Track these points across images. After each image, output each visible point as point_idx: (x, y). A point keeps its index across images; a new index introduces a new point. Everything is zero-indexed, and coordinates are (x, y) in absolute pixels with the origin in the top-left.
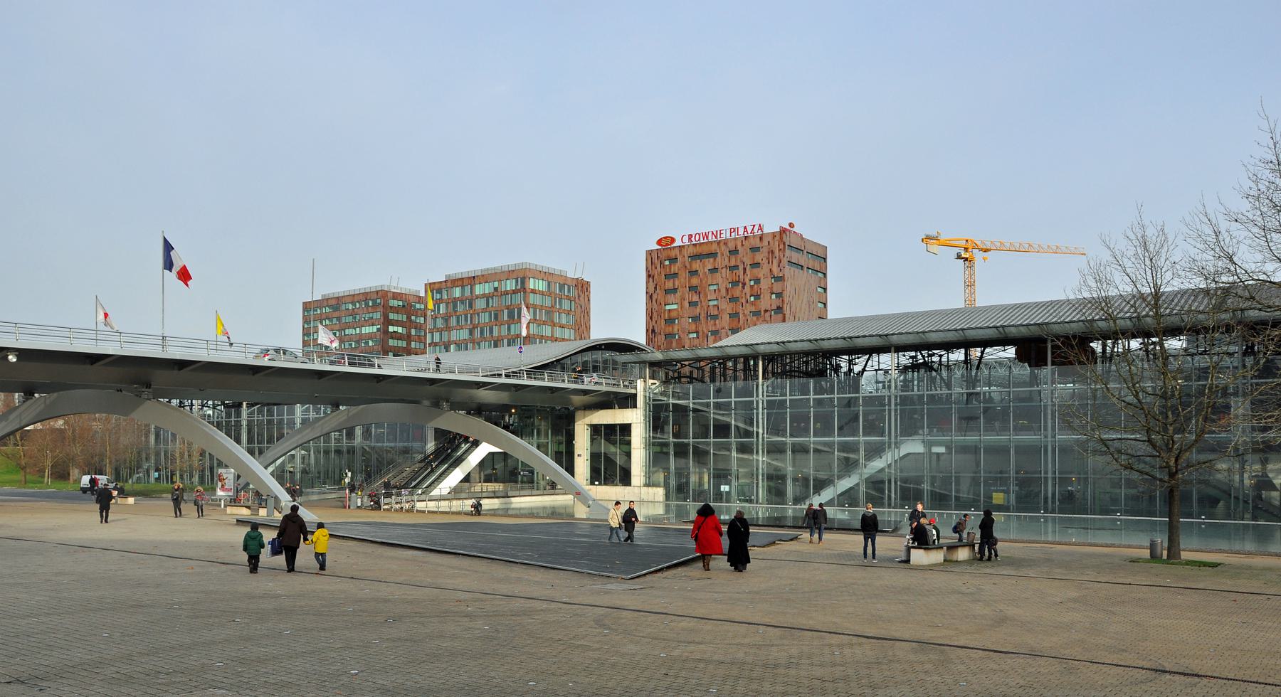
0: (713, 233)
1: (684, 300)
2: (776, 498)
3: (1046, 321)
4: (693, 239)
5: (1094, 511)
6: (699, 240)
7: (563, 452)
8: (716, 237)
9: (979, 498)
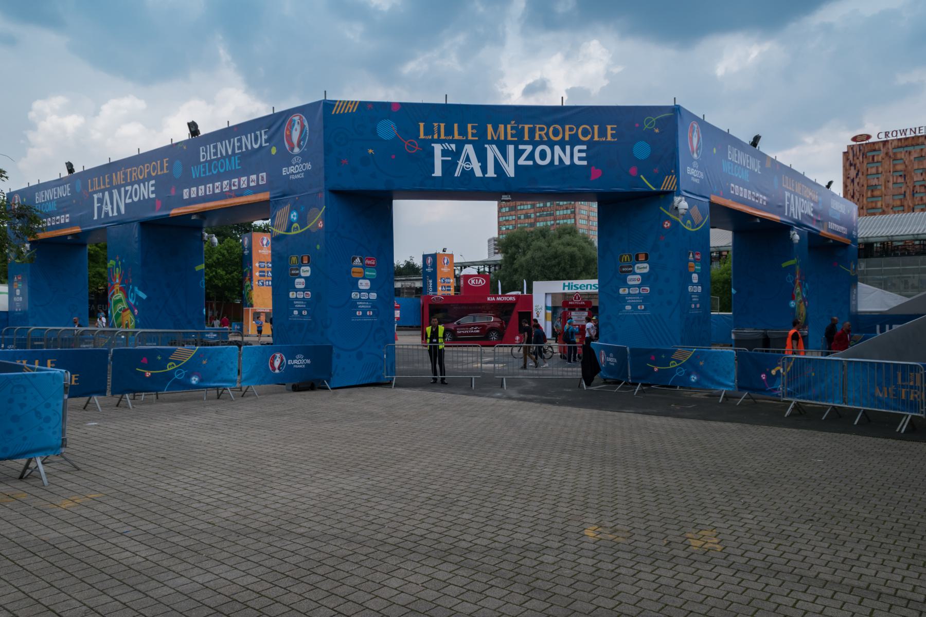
0: (911, 129)
1: (888, 182)
2: (788, 346)
3: (866, 235)
4: (890, 135)
5: (915, 369)
6: (896, 136)
7: (127, 346)
8: (915, 133)
9: (794, 359)
